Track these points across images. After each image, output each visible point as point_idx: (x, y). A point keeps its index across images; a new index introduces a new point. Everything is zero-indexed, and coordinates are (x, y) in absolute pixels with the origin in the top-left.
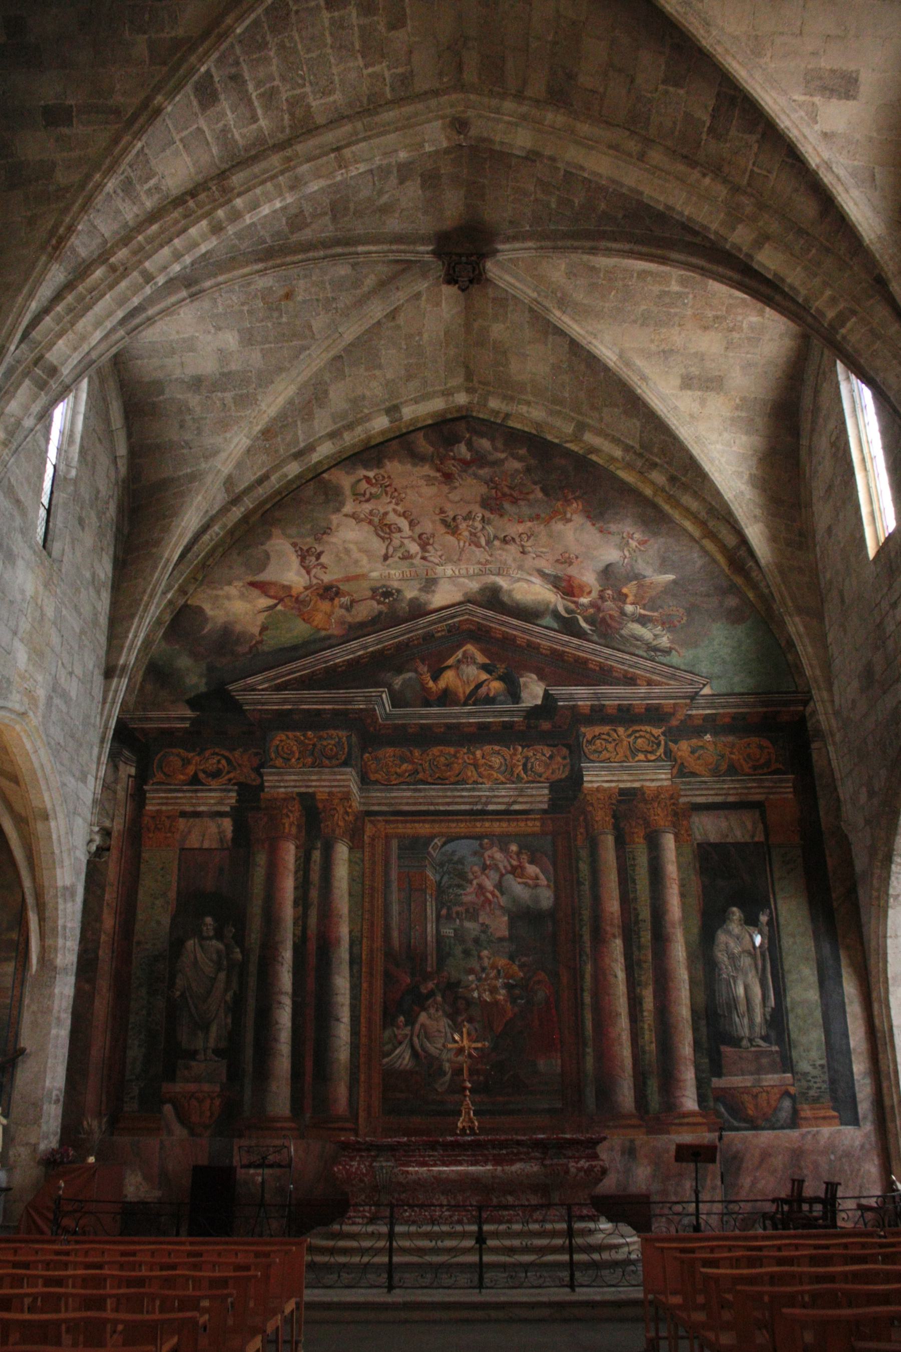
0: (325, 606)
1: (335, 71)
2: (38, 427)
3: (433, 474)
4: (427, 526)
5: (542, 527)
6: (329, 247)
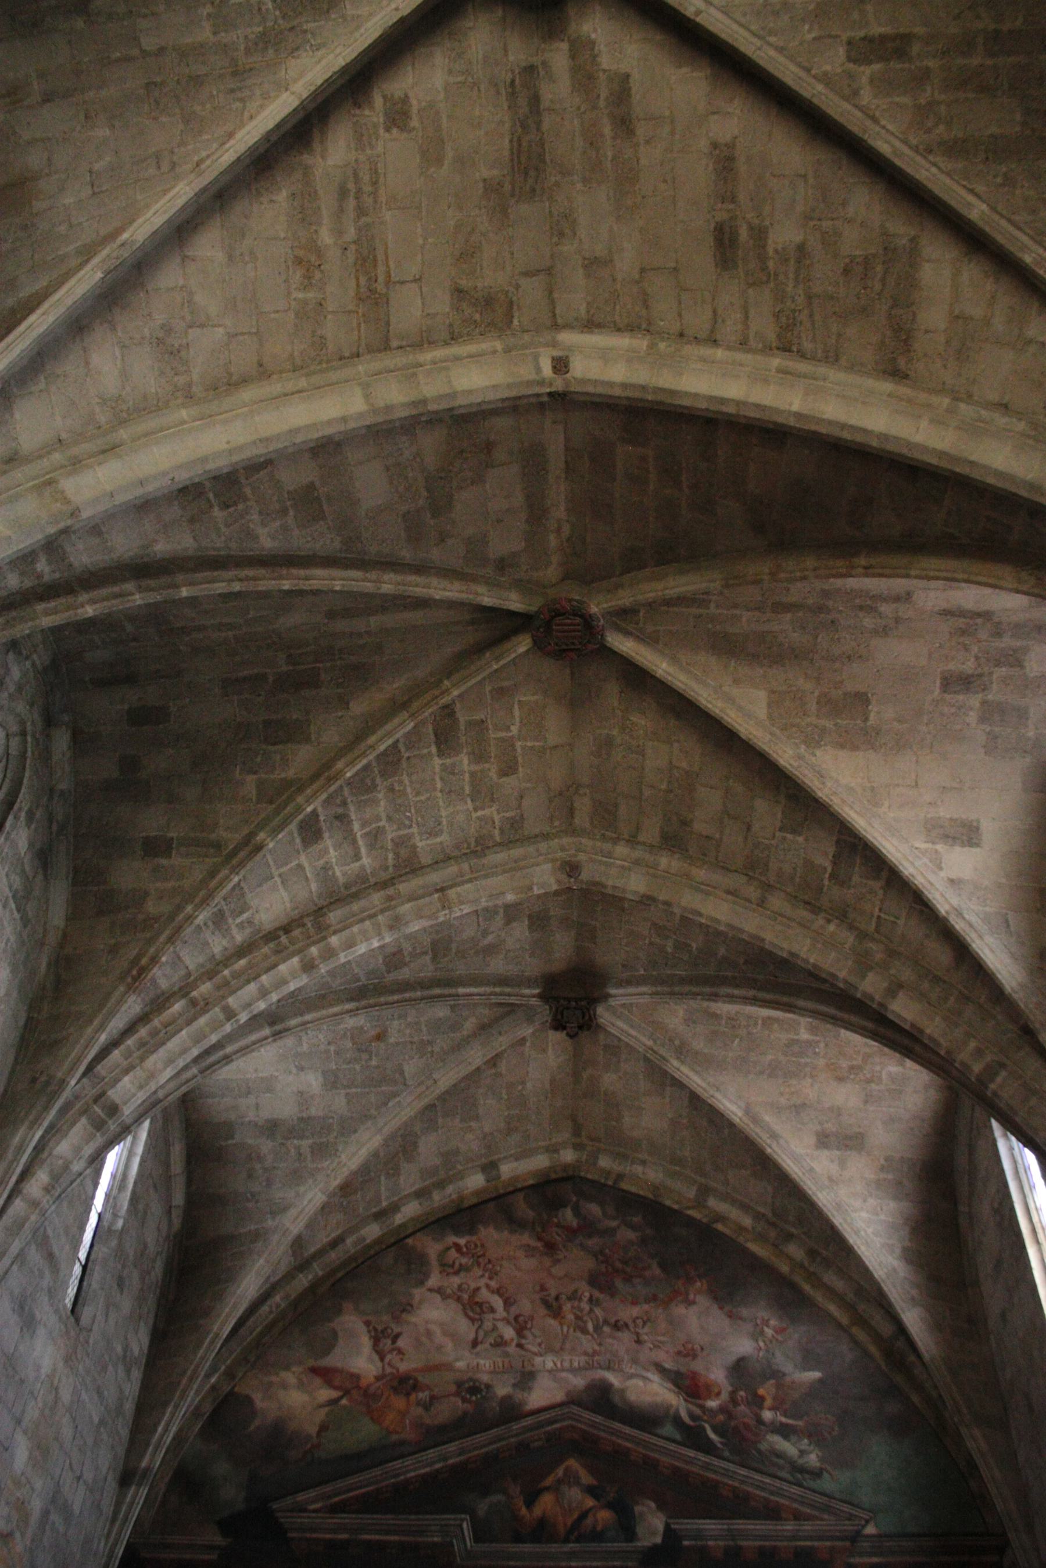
0: (399, 1402)
1: (443, 813)
2: (88, 1171)
3: (534, 1243)
4: (525, 1306)
5: (660, 1311)
6: (428, 988)
